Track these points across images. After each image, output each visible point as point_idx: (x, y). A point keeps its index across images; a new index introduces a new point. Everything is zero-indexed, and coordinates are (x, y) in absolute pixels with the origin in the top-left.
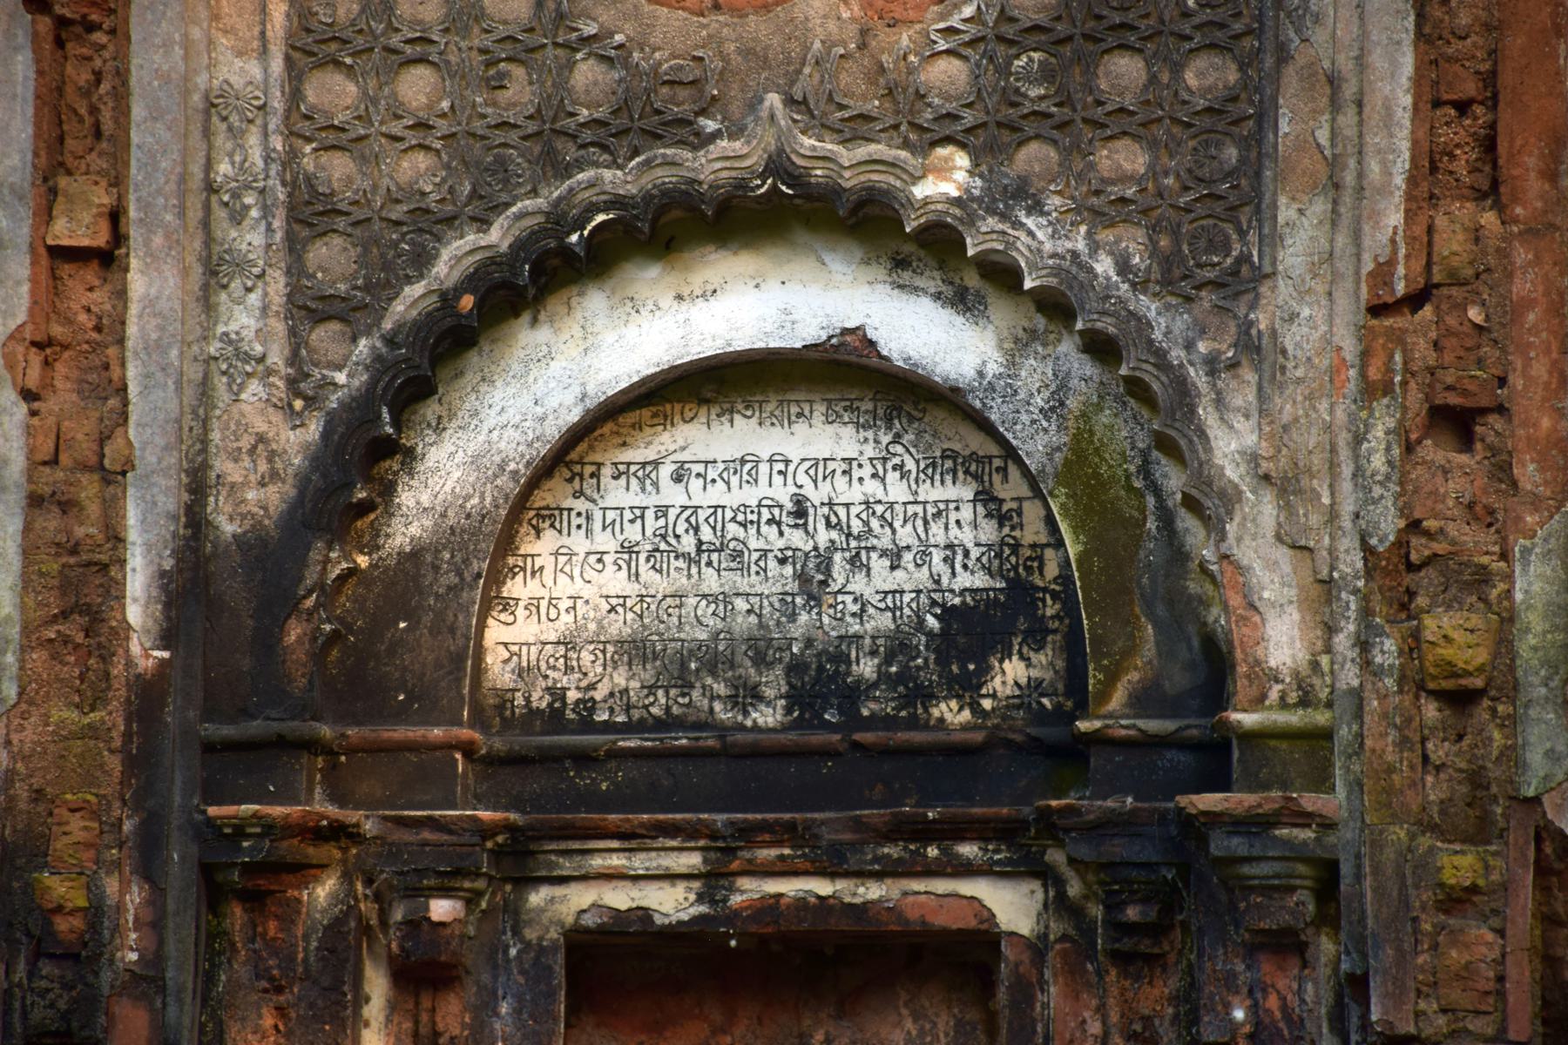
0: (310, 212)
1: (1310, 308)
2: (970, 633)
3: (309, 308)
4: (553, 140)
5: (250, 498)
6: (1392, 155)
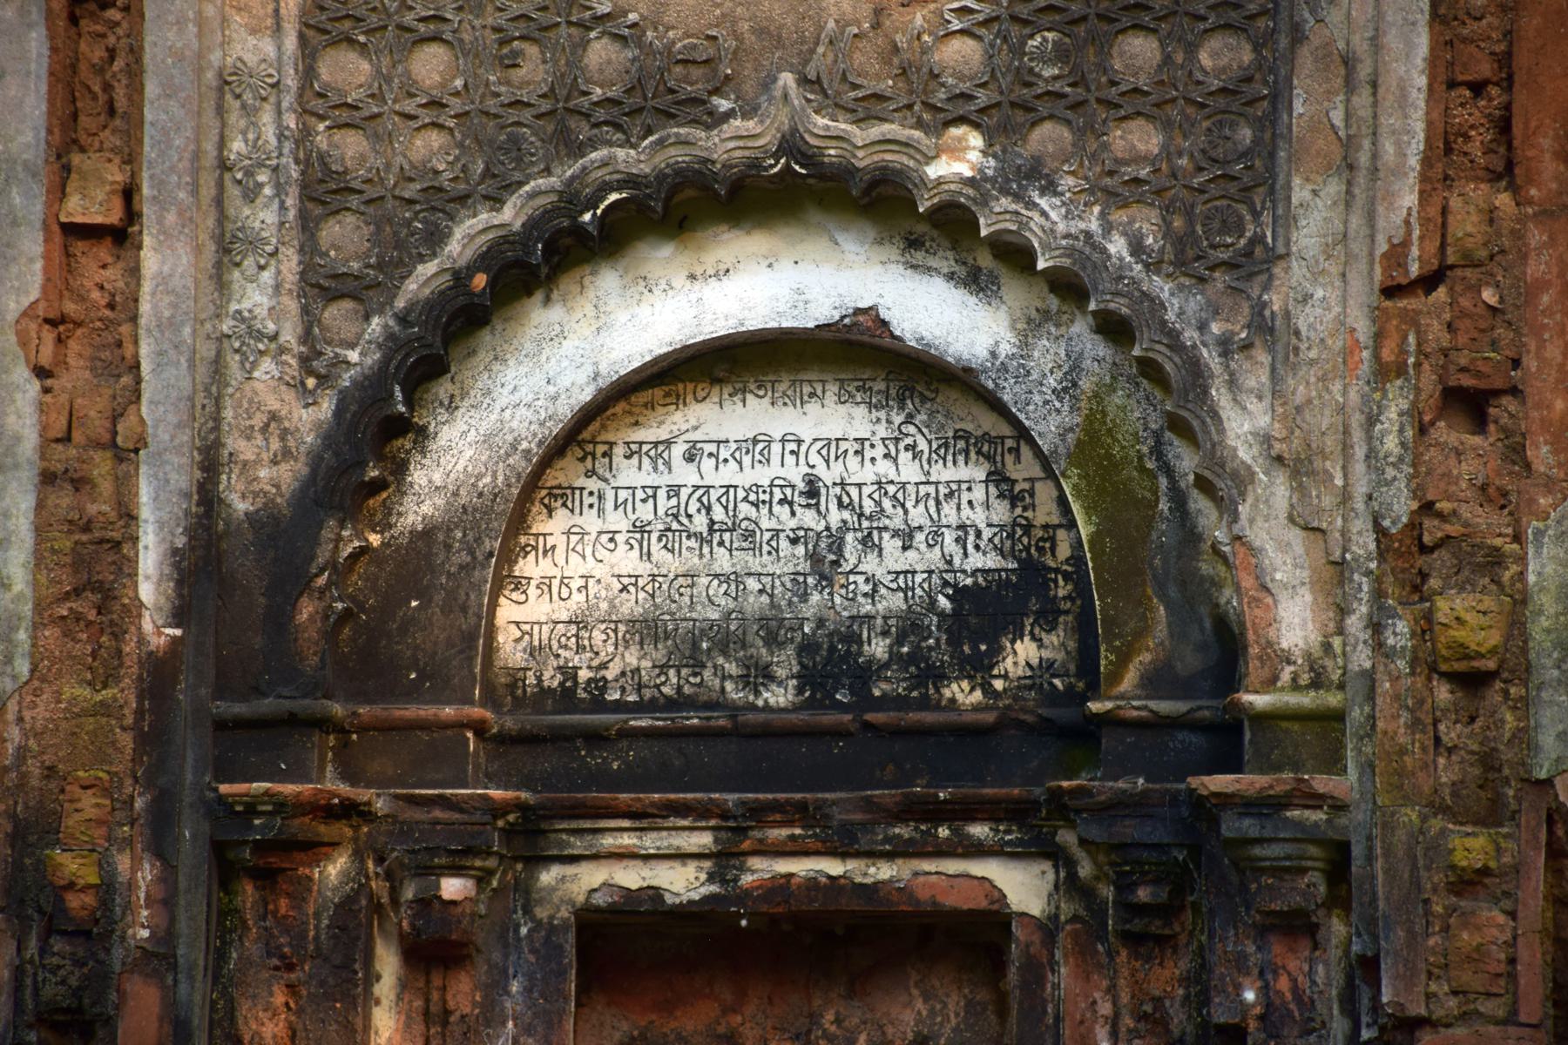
0: (323, 191)
1: (1324, 289)
2: (982, 613)
3: (322, 286)
4: (567, 119)
5: (263, 476)
6: (1406, 136)
